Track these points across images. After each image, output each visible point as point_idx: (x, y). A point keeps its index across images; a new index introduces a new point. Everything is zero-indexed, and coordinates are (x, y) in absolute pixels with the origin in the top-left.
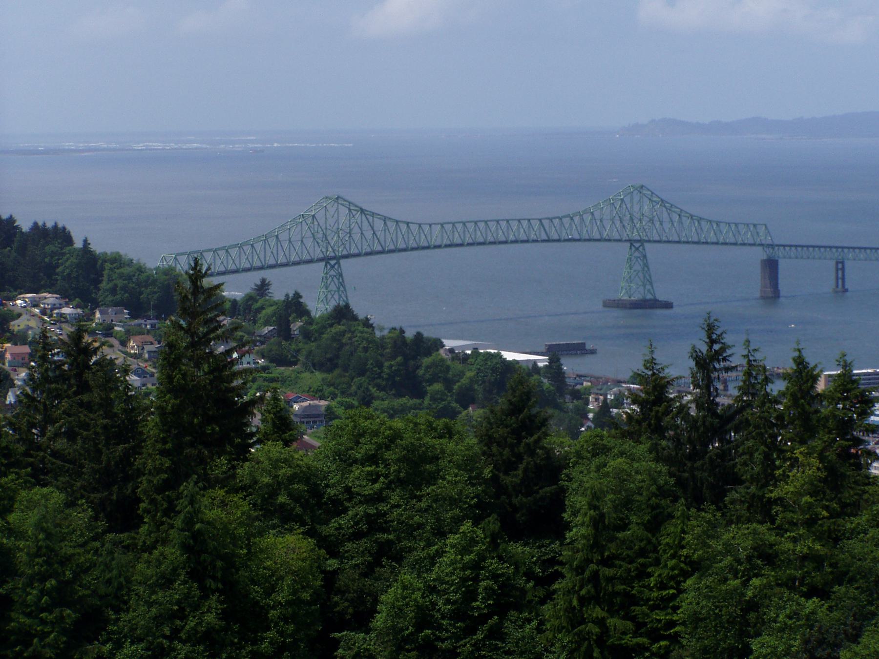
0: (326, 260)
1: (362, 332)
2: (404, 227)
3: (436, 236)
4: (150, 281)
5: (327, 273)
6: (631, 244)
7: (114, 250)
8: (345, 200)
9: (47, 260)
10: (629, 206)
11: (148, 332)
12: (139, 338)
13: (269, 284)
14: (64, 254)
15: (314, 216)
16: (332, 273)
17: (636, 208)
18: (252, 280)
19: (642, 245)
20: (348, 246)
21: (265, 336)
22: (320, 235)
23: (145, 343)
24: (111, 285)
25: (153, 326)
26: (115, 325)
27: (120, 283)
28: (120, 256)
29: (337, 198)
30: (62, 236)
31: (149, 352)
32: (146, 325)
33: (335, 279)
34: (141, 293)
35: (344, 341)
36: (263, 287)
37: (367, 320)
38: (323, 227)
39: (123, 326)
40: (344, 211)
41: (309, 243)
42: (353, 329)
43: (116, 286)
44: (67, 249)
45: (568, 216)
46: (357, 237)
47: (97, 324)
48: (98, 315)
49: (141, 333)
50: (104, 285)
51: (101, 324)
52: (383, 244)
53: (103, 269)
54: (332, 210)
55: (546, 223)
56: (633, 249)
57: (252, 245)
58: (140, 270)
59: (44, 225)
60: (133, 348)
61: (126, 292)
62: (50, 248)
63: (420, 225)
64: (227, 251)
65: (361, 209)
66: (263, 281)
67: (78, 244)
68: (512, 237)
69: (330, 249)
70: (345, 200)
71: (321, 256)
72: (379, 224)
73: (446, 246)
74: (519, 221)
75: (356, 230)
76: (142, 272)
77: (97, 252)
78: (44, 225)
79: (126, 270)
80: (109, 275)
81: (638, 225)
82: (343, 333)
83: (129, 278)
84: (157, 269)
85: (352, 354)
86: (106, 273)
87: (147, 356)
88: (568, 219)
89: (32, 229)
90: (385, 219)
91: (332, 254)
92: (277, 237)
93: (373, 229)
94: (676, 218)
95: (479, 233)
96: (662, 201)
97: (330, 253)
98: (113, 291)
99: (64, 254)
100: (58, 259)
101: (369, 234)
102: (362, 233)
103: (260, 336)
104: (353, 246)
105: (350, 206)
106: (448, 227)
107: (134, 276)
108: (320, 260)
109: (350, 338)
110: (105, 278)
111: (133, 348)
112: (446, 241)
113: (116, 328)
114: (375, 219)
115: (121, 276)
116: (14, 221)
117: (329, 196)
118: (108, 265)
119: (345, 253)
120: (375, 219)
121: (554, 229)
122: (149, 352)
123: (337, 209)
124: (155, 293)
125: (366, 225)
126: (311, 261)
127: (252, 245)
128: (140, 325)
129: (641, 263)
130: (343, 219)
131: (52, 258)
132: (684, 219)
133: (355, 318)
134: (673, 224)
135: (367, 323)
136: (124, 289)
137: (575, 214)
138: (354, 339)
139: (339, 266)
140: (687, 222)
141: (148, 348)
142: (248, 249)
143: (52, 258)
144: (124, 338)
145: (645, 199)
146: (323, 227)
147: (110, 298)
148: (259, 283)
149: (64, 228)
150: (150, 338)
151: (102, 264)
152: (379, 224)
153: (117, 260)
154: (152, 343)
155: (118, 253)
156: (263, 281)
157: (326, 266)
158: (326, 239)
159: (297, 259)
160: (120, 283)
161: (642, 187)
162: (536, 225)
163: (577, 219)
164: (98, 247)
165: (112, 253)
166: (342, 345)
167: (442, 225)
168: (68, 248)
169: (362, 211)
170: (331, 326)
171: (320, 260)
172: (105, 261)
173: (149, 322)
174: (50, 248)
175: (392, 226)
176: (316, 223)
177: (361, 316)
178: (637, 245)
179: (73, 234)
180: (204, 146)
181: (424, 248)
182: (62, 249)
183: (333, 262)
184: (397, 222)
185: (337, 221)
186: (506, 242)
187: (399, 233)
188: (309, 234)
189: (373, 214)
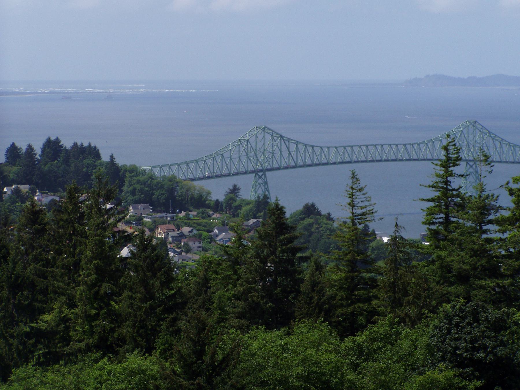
0: (255, 172)
1: (326, 224)
2: (310, 149)
3: (402, 153)
4: (159, 186)
5: (256, 182)
6: (467, 163)
7: (132, 163)
8: (270, 129)
9: (84, 170)
10: (466, 135)
11: (169, 222)
12: (164, 226)
13: (239, 189)
14: (96, 166)
15: (248, 141)
16: (260, 181)
17: (471, 137)
18: (227, 184)
19: (475, 163)
20: (271, 163)
21: (251, 226)
22: (252, 154)
23: (169, 230)
24: (131, 188)
25: (172, 218)
26: (144, 217)
27: (138, 187)
28: (136, 167)
29: (264, 128)
30: (93, 152)
31: (172, 237)
32: (167, 217)
33: (262, 185)
34: (153, 194)
35: (313, 230)
36: (235, 190)
37: (329, 214)
38: (254, 148)
39: (150, 218)
40: (269, 137)
41: (244, 159)
42: (319, 221)
43: (135, 189)
44: (98, 163)
45: (424, 142)
46: (277, 156)
47: (130, 216)
48: (131, 209)
49: (164, 223)
50: (125, 188)
51: (134, 216)
52: (295, 160)
53: (125, 177)
54: (260, 137)
55: (408, 146)
56: (468, 166)
57: (205, 161)
58: (152, 177)
59: (82, 145)
60: (160, 233)
61: (142, 193)
62: (86, 161)
63: (321, 148)
64: (187, 165)
65: (281, 135)
66: (235, 186)
67: (105, 158)
68: (384, 157)
69: (259, 164)
70: (270, 129)
71: (253, 169)
72: (293, 147)
73: (340, 163)
74: (321, 148)
75: (277, 151)
76: (153, 179)
77: (120, 165)
78: (82, 145)
79: (141, 178)
80: (130, 182)
81: (472, 150)
82: (311, 225)
83: (144, 183)
84: (164, 177)
85: (319, 240)
86: (127, 180)
87: (171, 239)
88: (423, 145)
89: (72, 148)
90: (297, 143)
91: (260, 168)
92: (222, 155)
93: (289, 151)
94: (498, 144)
95: (362, 154)
96: (489, 132)
97: (259, 167)
98: (133, 193)
99: (96, 166)
100: (93, 169)
101: (286, 154)
102: (281, 153)
103: (247, 226)
104: (275, 162)
105: (273, 133)
106: (341, 150)
107: (147, 182)
108: (251, 172)
109: (317, 228)
110: (127, 183)
111: (160, 233)
112: (339, 160)
113: (144, 219)
114: (291, 144)
115: (138, 182)
116: (60, 142)
117: (258, 126)
118: (128, 174)
119: (269, 167)
120: (291, 144)
121: (414, 151)
122: (172, 237)
123: (264, 137)
124: (163, 194)
125: (284, 147)
126: (246, 173)
127: (205, 161)
128: (162, 217)
129: (475, 177)
130: (268, 143)
131: (88, 168)
132: (504, 145)
133: (319, 214)
134: (496, 149)
135: (329, 217)
136: (141, 191)
137: (429, 141)
138: (321, 229)
139: (265, 176)
140: (506, 148)
141: (171, 234)
142: (202, 164)
143: (88, 168)
144: (151, 226)
145: (477, 131)
146: (254, 148)
147: (130, 198)
148: (231, 188)
149: (95, 147)
150: (172, 227)
151: (124, 173)
152: (293, 147)
153: (133, 170)
154: (174, 231)
155: (134, 165)
156: (235, 186)
157: (255, 176)
158: (256, 157)
159: (201, 175)
160: (138, 187)
161: (475, 122)
162: (402, 149)
163: (430, 144)
164: (120, 161)
165: (131, 165)
166: (311, 234)
167: (336, 148)
168: (99, 162)
169: (282, 137)
170: (303, 219)
171: (251, 172)
172: (125, 171)
173: (168, 215)
174: (86, 161)
175: (302, 148)
176: (249, 145)
177: (324, 212)
178: (471, 163)
179: (101, 152)
180: (97, 90)
181: (324, 164)
182: (95, 162)
183: (260, 174)
184: (306, 145)
185: (264, 144)
186: (380, 161)
187: (307, 154)
188: (244, 154)
189: (289, 140)
